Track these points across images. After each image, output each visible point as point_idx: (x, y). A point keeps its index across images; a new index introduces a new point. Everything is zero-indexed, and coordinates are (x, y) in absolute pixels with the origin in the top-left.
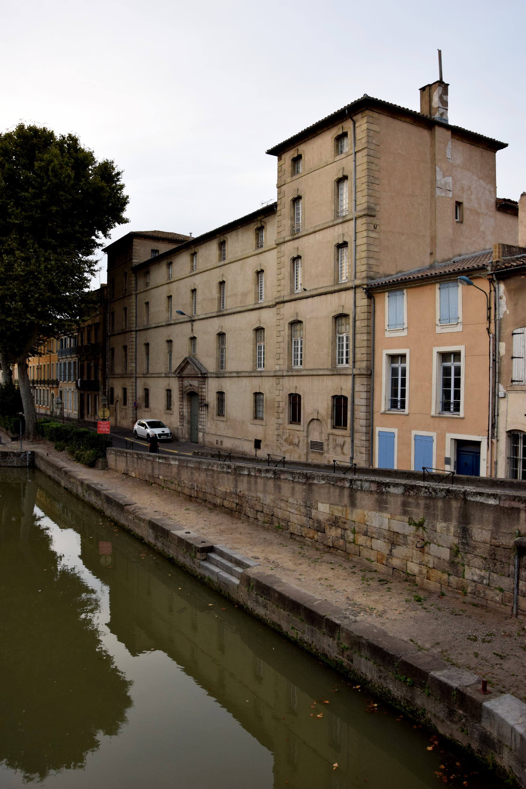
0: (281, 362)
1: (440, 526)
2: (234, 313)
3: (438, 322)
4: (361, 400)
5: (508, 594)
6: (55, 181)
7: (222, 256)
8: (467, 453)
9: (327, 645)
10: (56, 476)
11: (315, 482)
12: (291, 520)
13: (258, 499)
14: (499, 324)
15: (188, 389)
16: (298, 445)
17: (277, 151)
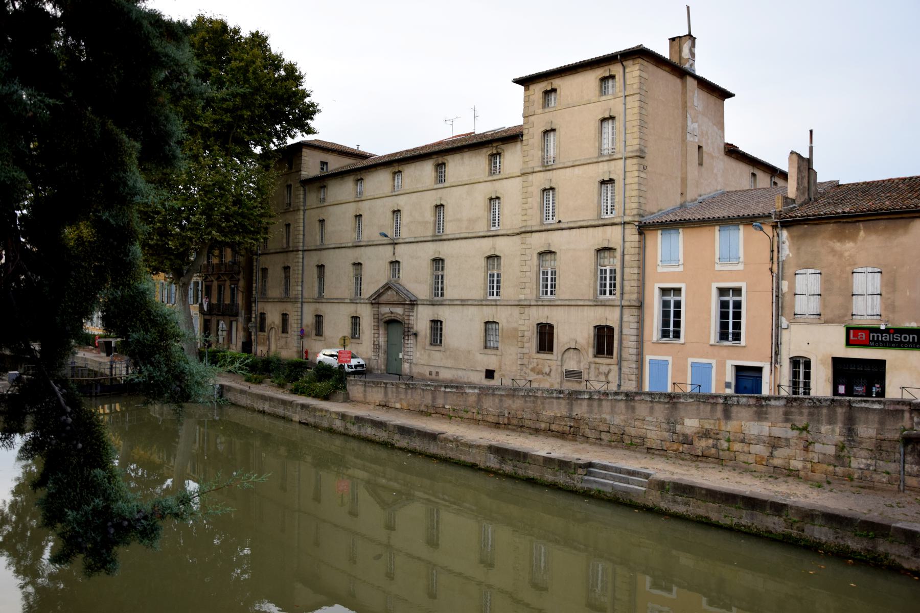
0: (527, 291)
1: (825, 428)
2: (453, 239)
3: (717, 260)
4: (630, 330)
5: (894, 476)
6: (255, 84)
7: (441, 178)
8: (747, 378)
9: (775, 524)
10: (280, 411)
11: (681, 400)
12: (648, 436)
13: (603, 421)
14: (781, 265)
15: (387, 317)
16: (549, 374)
17: (525, 82)
